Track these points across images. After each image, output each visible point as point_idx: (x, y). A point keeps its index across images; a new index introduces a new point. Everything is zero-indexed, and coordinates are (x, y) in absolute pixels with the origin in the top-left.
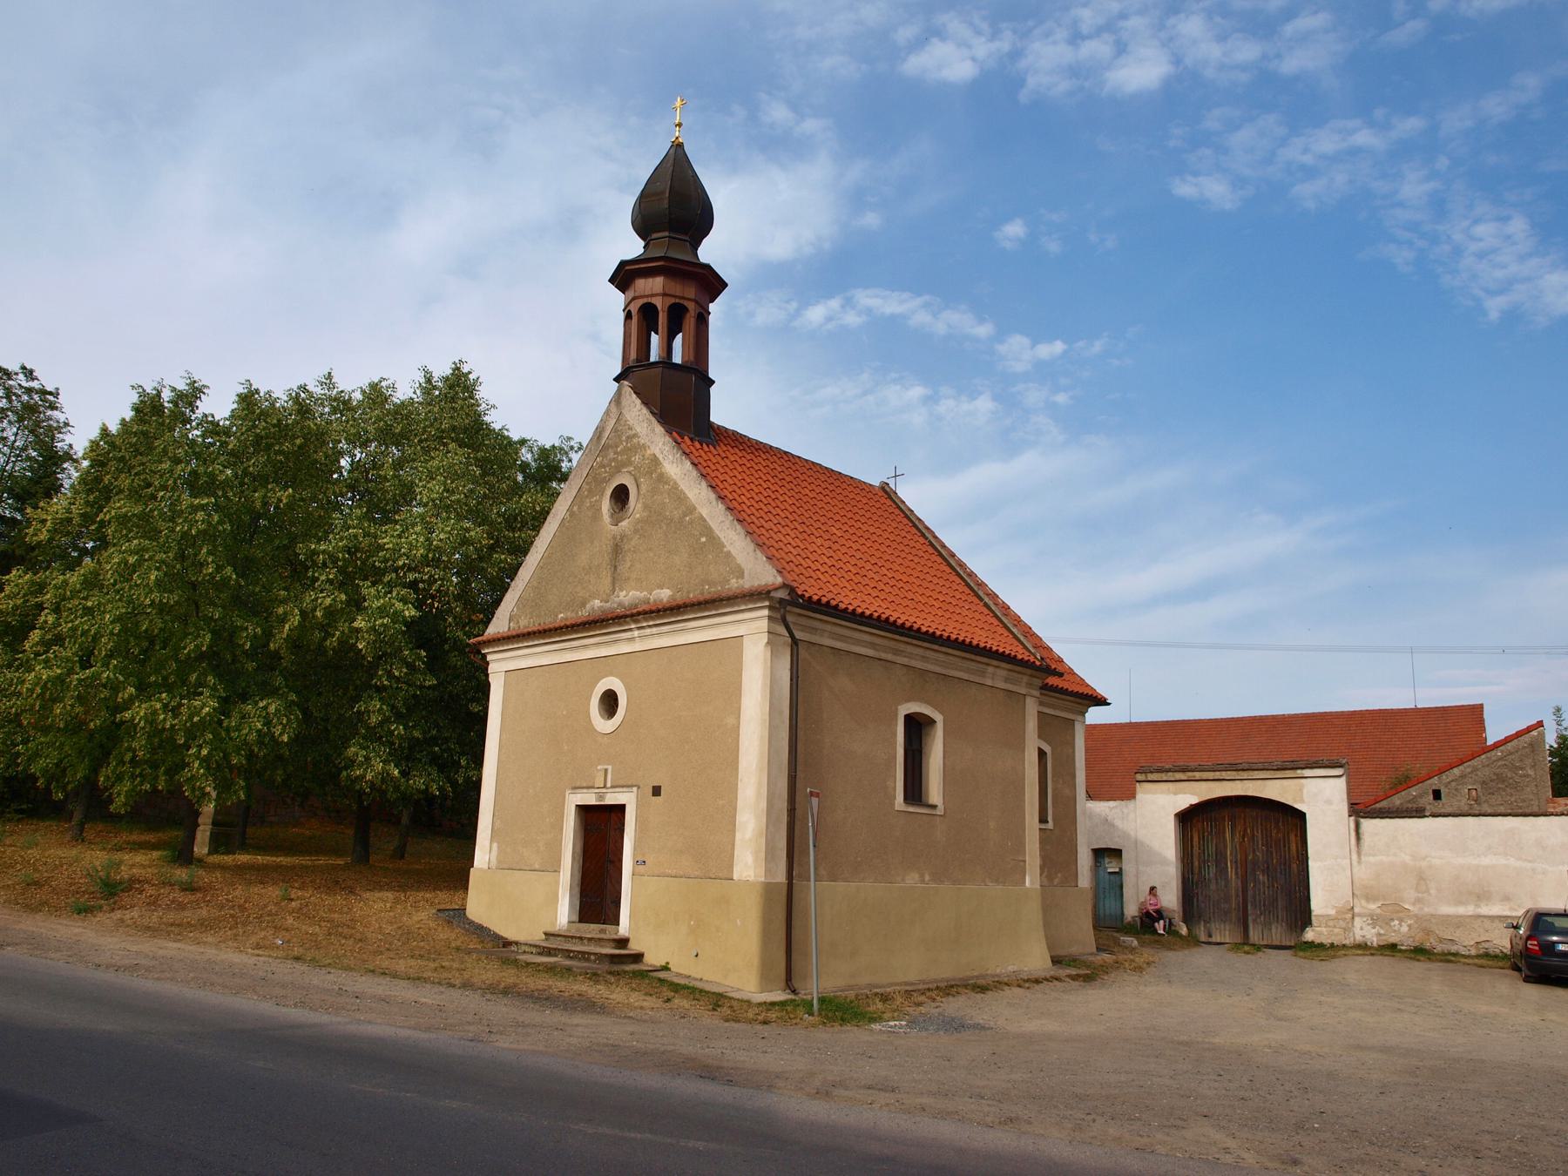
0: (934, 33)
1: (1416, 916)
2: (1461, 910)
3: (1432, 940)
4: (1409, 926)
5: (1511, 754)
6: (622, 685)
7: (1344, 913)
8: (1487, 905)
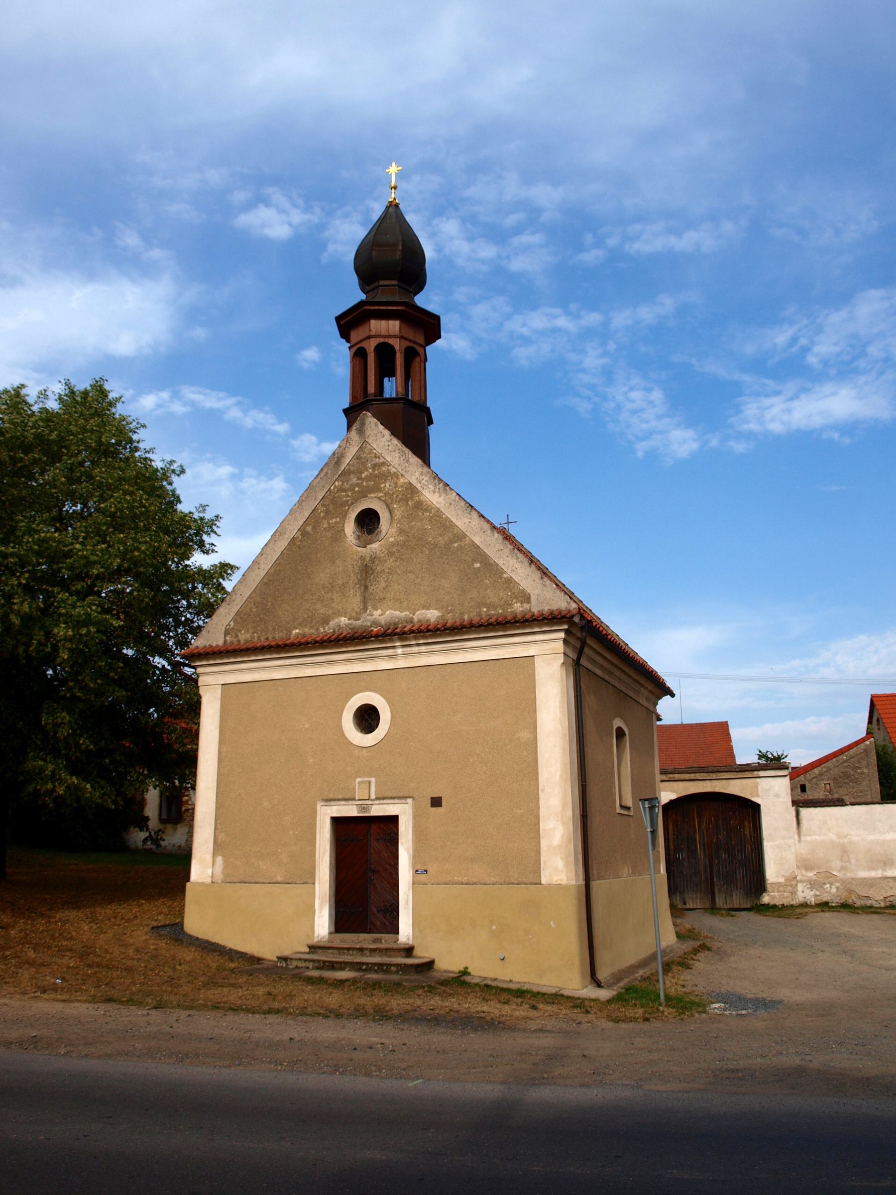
0: (262, 200)
1: (841, 880)
2: (873, 874)
3: (853, 898)
4: (837, 888)
5: (853, 757)
6: (385, 701)
7: (791, 880)
8: (891, 869)
